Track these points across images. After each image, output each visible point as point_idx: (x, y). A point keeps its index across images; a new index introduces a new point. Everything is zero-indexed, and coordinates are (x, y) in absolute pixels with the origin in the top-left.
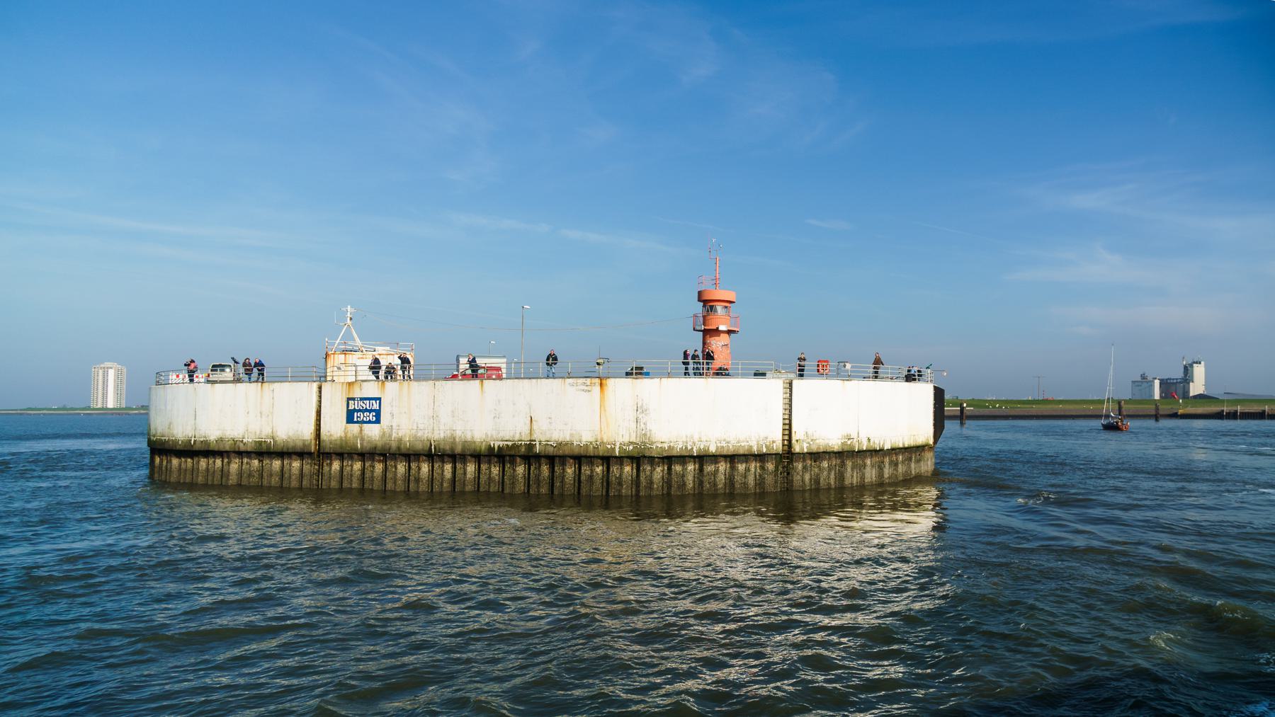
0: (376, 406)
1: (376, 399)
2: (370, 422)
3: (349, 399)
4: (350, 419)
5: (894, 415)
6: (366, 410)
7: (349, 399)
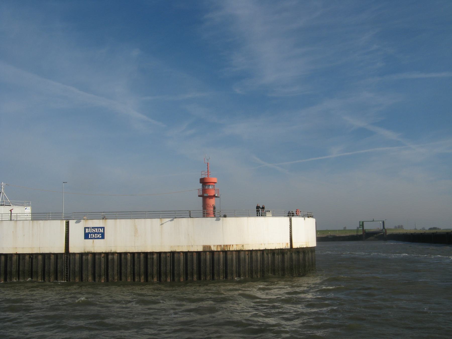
0: (101, 231)
1: (101, 228)
2: (98, 238)
3: (85, 228)
4: (87, 236)
5: (304, 234)
6: (96, 233)
7: (104, 228)
